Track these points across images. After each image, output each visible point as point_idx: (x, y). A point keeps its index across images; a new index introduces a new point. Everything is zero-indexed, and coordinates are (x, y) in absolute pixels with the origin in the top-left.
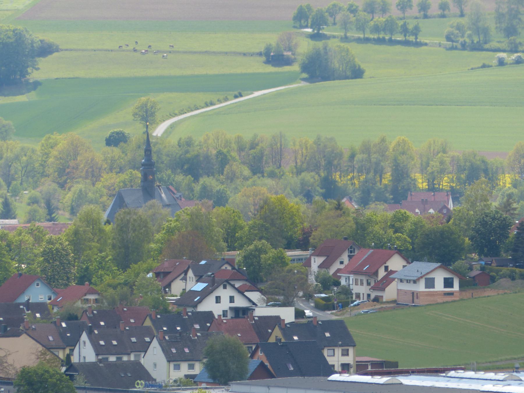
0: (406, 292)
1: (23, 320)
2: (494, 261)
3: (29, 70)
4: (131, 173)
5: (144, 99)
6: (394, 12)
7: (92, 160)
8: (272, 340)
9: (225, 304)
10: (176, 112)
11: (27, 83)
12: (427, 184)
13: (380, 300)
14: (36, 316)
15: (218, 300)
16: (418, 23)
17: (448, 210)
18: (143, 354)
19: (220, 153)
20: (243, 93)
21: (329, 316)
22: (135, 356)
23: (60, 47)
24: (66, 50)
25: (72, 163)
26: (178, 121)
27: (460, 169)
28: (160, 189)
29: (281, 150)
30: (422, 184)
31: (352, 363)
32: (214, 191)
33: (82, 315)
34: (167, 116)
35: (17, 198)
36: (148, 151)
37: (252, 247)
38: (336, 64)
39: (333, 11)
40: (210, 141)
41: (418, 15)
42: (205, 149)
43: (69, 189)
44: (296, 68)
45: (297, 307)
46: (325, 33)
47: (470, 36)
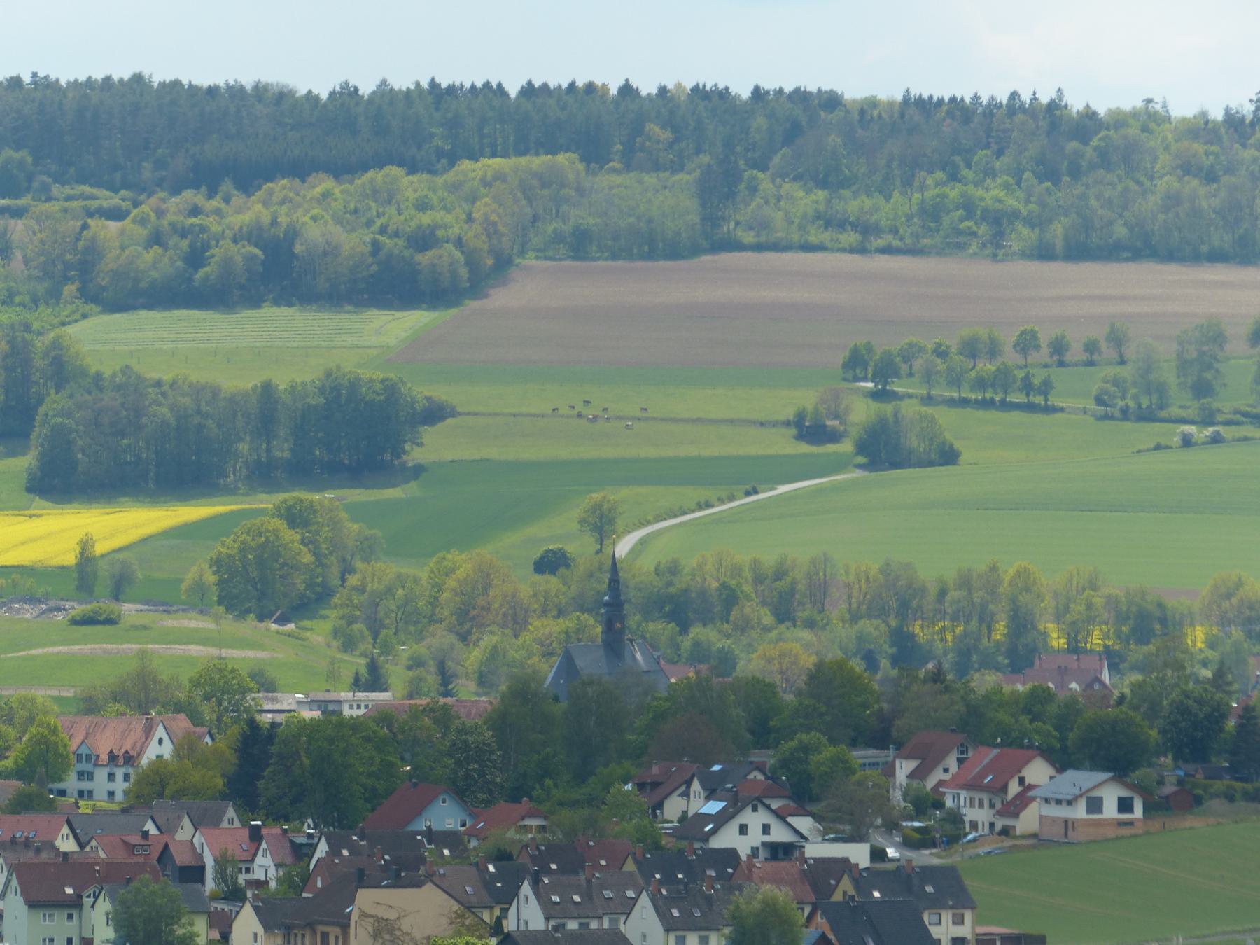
0: (1054, 820)
1: (423, 860)
2: (1200, 770)
3: (407, 447)
4: (578, 619)
5: (596, 496)
6: (1011, 357)
7: (514, 596)
8: (837, 897)
9: (755, 837)
10: (650, 518)
11: (403, 466)
12: (1065, 640)
13: (1011, 832)
14: (443, 853)
15: (743, 830)
16: (1049, 376)
17: (1102, 684)
18: (623, 918)
19: (724, 586)
20: (760, 488)
21: (927, 857)
22: (610, 921)
23: (458, 409)
24: (469, 414)
25: (481, 601)
26: (652, 532)
27: (1121, 618)
28: (633, 646)
29: (825, 584)
30: (1058, 641)
31: (969, 936)
32: (714, 649)
33: (521, 852)
34: (635, 525)
35: (390, 658)
36: (615, 582)
37: (792, 744)
38: (913, 442)
39: (908, 355)
40: (709, 567)
41: (1048, 360)
42: (699, 580)
43: (476, 644)
44: (847, 447)
45: (874, 843)
46: (895, 389)
47: (1135, 397)
